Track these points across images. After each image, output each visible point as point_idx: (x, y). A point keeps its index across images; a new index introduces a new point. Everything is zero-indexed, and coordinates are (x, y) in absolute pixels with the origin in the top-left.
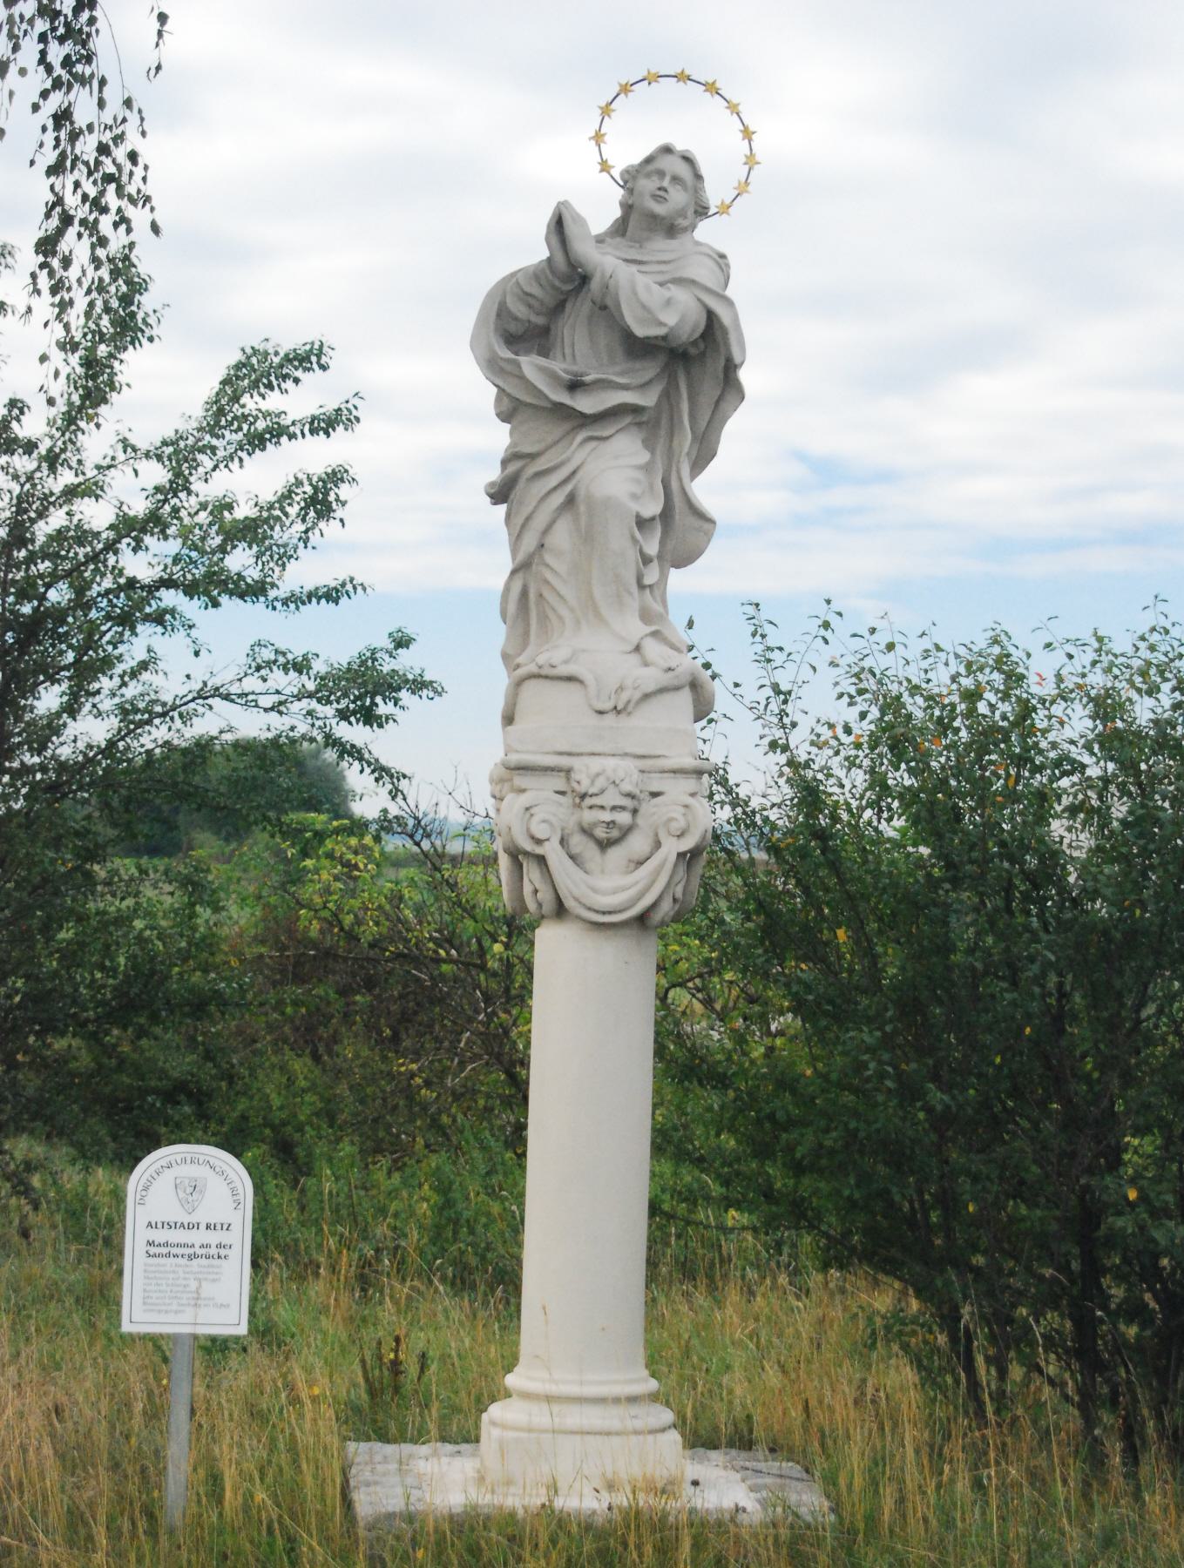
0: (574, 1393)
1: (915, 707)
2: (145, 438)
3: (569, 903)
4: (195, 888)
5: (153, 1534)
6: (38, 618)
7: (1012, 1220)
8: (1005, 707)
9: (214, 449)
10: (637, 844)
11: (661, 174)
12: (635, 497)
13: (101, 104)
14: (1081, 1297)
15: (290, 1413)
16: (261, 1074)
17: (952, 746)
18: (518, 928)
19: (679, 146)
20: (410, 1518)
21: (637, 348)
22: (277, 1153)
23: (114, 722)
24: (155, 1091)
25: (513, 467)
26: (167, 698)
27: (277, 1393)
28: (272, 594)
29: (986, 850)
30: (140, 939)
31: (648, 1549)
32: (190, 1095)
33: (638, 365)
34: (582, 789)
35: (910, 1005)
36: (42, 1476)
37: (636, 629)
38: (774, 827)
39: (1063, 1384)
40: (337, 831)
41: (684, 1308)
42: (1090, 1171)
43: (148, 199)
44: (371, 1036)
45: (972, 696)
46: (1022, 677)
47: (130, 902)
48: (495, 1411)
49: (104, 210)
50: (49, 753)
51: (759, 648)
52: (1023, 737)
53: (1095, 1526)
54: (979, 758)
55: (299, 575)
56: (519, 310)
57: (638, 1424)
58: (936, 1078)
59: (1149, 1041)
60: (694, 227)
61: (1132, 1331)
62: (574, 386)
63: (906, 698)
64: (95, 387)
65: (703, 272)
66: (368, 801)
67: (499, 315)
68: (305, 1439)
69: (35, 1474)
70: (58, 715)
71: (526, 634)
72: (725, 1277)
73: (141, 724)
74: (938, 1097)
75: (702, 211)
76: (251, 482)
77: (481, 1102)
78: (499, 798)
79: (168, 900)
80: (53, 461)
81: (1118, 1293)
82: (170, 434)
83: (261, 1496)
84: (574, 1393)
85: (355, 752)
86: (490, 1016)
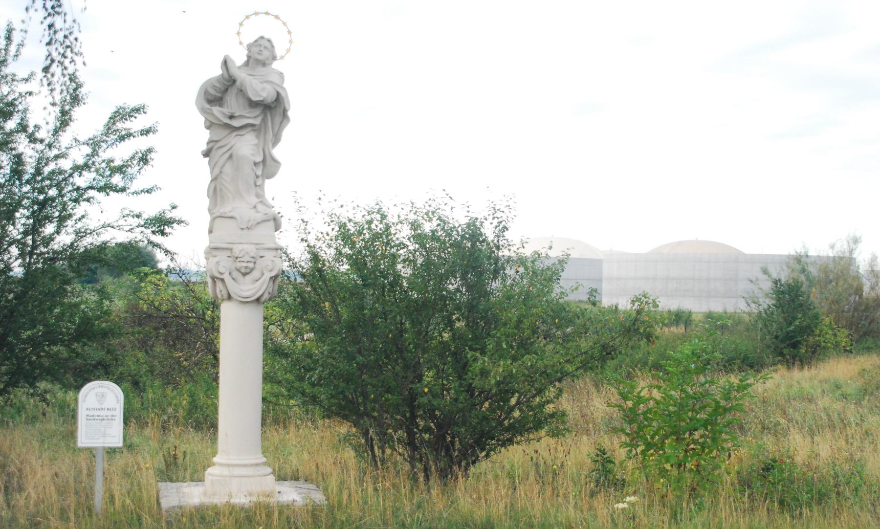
0: (237, 465)
1: (351, 227)
2: (82, 139)
3: (232, 295)
4: (103, 294)
5: (90, 515)
6: (46, 201)
7: (387, 400)
8: (381, 226)
9: (107, 141)
10: (256, 274)
11: (260, 45)
12: (253, 155)
13: (65, 21)
14: (410, 425)
15: (138, 474)
16: (127, 358)
17: (363, 240)
18: (215, 306)
19: (266, 36)
20: (181, 508)
21: (253, 104)
22: (133, 385)
23: (73, 236)
24: (90, 364)
25: (211, 145)
26: (92, 227)
27: (133, 466)
28: (128, 191)
29: (375, 275)
30: (83, 311)
31: (264, 515)
32: (102, 366)
33: (253, 110)
34: (236, 255)
35: (351, 328)
36: (51, 497)
37: (254, 200)
38: (303, 268)
39: (404, 455)
40: (152, 273)
41: (276, 434)
42: (412, 382)
43: (81, 54)
44: (161, 342)
45: (370, 222)
46: (386, 216)
47: (79, 299)
48: (210, 470)
49: (65, 57)
50: (50, 247)
51: (297, 207)
52: (387, 237)
53: (415, 501)
54: (372, 244)
55: (136, 185)
56: (212, 92)
57: (259, 473)
58: (360, 352)
59: (432, 338)
60: (271, 64)
61: (426, 436)
62: (232, 117)
63: (348, 224)
64: (64, 120)
65: (275, 79)
66: (163, 261)
67: (205, 93)
68: (144, 482)
69: (48, 496)
70: (53, 234)
71: (216, 200)
72: (290, 423)
73: (82, 237)
74: (360, 358)
75: (274, 58)
76: (120, 153)
77: (205, 366)
78: (207, 259)
79: (92, 297)
80: (50, 146)
81: (422, 423)
82: (91, 136)
83: (128, 501)
84: (237, 465)
85: (158, 246)
86: (207, 336)
